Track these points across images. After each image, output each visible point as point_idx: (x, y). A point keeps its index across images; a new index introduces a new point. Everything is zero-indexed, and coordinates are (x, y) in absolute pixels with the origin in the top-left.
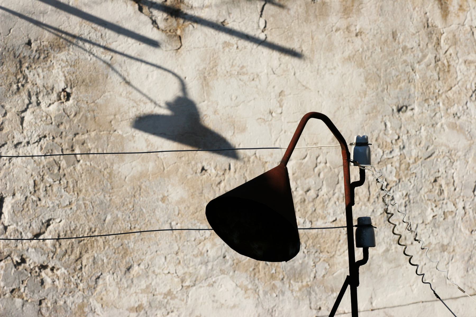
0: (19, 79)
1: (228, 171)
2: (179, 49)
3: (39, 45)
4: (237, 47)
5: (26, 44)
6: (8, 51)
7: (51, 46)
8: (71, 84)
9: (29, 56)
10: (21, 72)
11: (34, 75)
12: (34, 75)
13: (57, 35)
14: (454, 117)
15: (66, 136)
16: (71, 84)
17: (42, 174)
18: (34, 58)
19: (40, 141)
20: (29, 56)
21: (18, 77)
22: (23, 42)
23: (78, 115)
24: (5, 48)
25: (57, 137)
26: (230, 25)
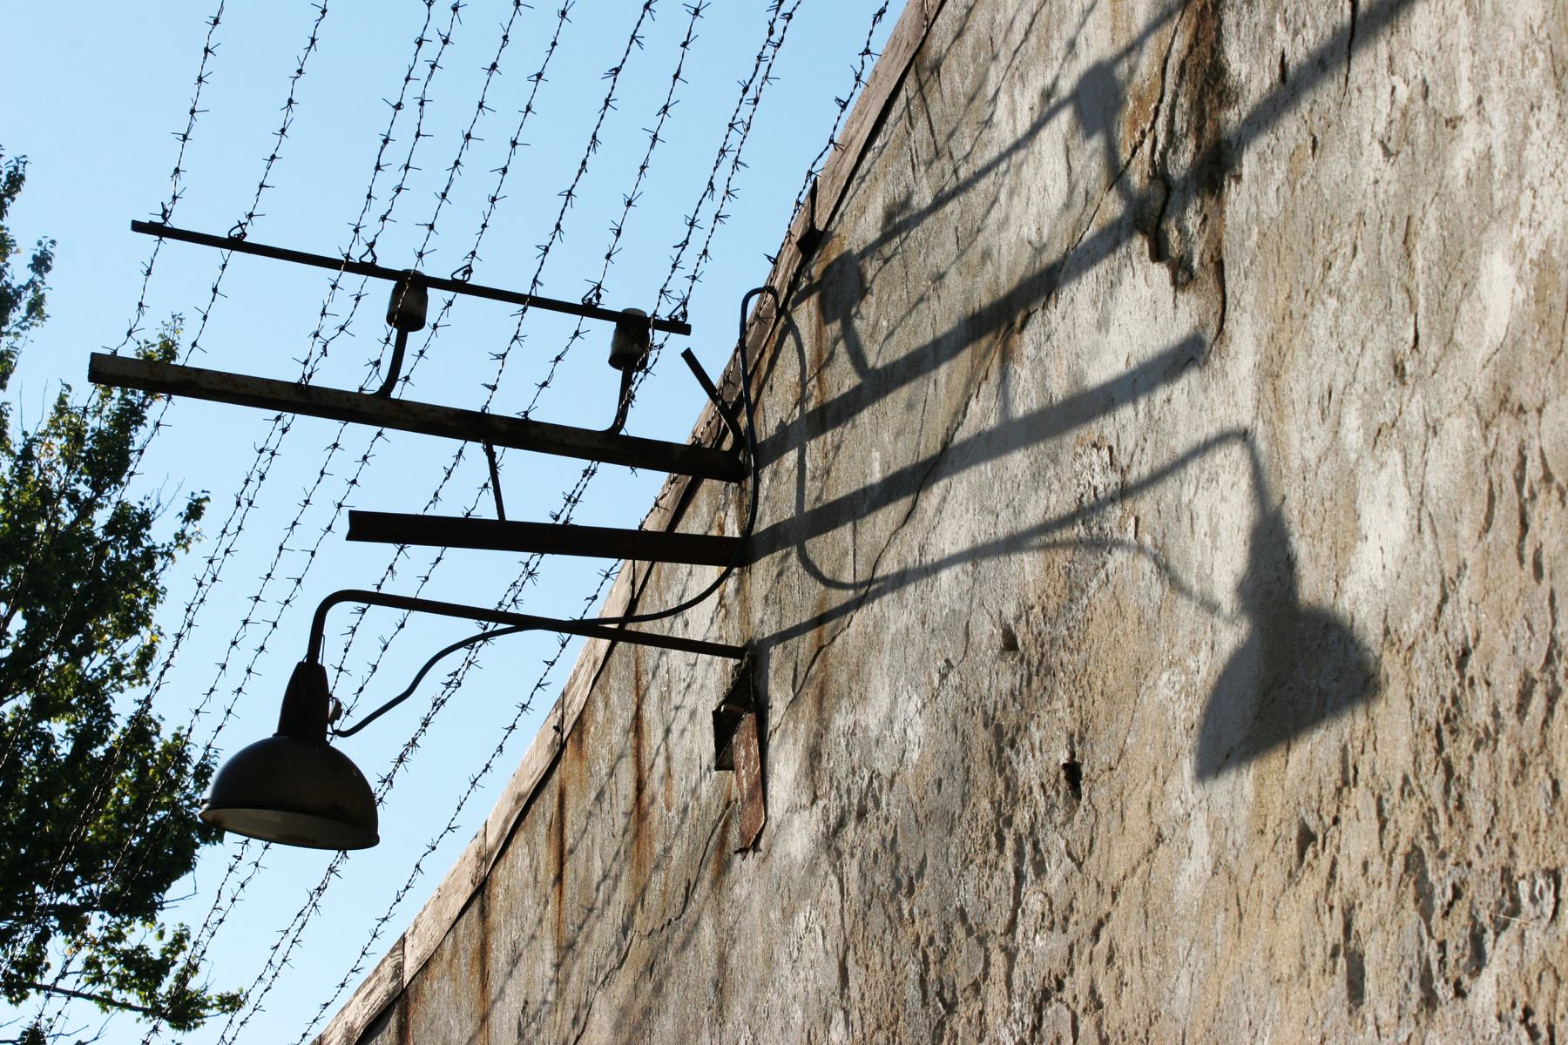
5: (1002, 651)
13: (1046, 547)
24: (967, 710)
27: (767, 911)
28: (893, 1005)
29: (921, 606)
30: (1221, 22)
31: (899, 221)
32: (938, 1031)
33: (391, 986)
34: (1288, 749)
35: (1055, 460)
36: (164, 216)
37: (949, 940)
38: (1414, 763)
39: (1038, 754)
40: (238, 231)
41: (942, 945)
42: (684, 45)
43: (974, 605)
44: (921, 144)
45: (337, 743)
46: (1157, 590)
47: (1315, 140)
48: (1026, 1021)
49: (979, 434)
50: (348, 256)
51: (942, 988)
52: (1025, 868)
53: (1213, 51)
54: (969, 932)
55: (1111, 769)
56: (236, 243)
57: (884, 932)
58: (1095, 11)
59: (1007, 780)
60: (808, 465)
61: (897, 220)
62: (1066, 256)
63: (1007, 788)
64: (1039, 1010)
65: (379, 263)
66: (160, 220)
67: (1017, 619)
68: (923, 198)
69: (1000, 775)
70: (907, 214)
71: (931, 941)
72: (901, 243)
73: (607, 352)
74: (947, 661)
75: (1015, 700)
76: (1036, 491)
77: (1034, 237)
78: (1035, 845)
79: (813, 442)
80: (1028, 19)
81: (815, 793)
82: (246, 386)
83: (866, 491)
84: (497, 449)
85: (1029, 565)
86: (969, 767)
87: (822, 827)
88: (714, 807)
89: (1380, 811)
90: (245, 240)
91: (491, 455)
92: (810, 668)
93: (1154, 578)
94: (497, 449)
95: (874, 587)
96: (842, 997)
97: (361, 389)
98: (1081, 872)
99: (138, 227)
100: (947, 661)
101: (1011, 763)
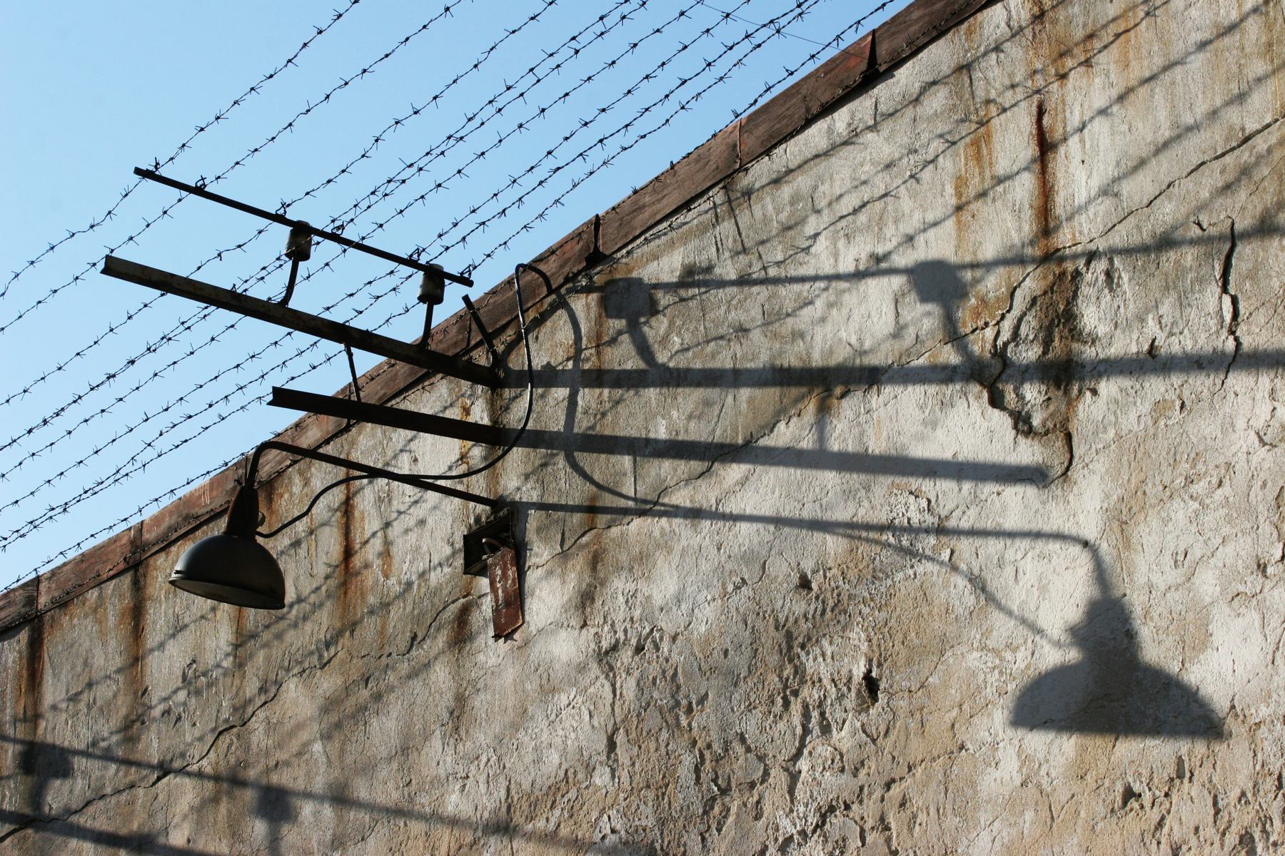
0: (787, 680)
1: (1177, 782)
2: (1068, 469)
3: (822, 580)
4: (1183, 406)
5: (797, 587)
6: (765, 618)
7: (843, 573)
8: (881, 655)
9: (805, 616)
10: (791, 661)
11: (815, 659)
12: (815, 659)
13: (851, 537)
14: (601, 660)
15: (870, 794)
16: (881, 655)
17: (1243, 818)
18: (814, 617)
19: (824, 823)
20: (805, 616)
21: (785, 674)
22: (792, 586)
23: (891, 731)
24: (758, 614)
25: (853, 803)
26: (1173, 346)
27: (522, 682)
28: (664, 777)
29: (717, 538)
30: (1077, 288)
31: (696, 278)
32: (710, 803)
33: (23, 610)
34: (1116, 739)
35: (868, 489)
36: (156, 167)
37: (727, 750)
38: (1254, 788)
39: (829, 660)
40: (201, 182)
41: (720, 751)
42: (566, 139)
43: (773, 552)
44: (727, 237)
45: (260, 540)
46: (970, 600)
47: (1183, 403)
48: (810, 820)
49: (788, 448)
50: (479, 309)
51: (717, 777)
52: (811, 726)
53: (1068, 303)
54: (748, 750)
55: (910, 691)
56: (199, 191)
57: (660, 730)
58: (938, 227)
59: (796, 668)
60: (580, 402)
61: (697, 278)
62: (890, 366)
63: (796, 672)
64: (823, 817)
65: (287, 216)
66: (152, 168)
67: (815, 572)
68: (728, 270)
69: (790, 663)
70: (707, 277)
71: (709, 746)
72: (700, 294)
73: (418, 292)
74: (742, 579)
75: (807, 620)
76: (846, 501)
77: (853, 341)
78: (822, 714)
79: (587, 390)
80: (858, 203)
81: (585, 621)
82: (201, 289)
83: (648, 441)
84: (353, 350)
85: (834, 545)
86: (757, 650)
87: (593, 646)
88: (445, 592)
89: (1215, 803)
90: (206, 189)
91: (350, 355)
92: (583, 535)
93: (967, 592)
94: (353, 350)
95: (657, 508)
96: (608, 757)
97: (270, 299)
98: (875, 745)
99: (138, 171)
100: (742, 579)
101: (799, 657)
